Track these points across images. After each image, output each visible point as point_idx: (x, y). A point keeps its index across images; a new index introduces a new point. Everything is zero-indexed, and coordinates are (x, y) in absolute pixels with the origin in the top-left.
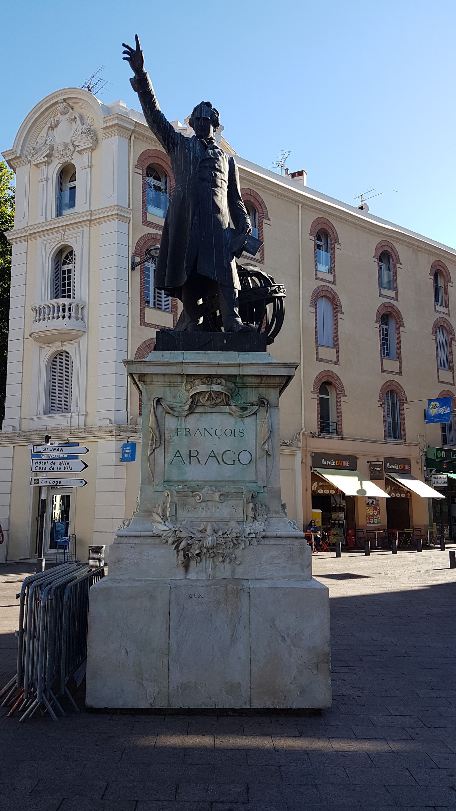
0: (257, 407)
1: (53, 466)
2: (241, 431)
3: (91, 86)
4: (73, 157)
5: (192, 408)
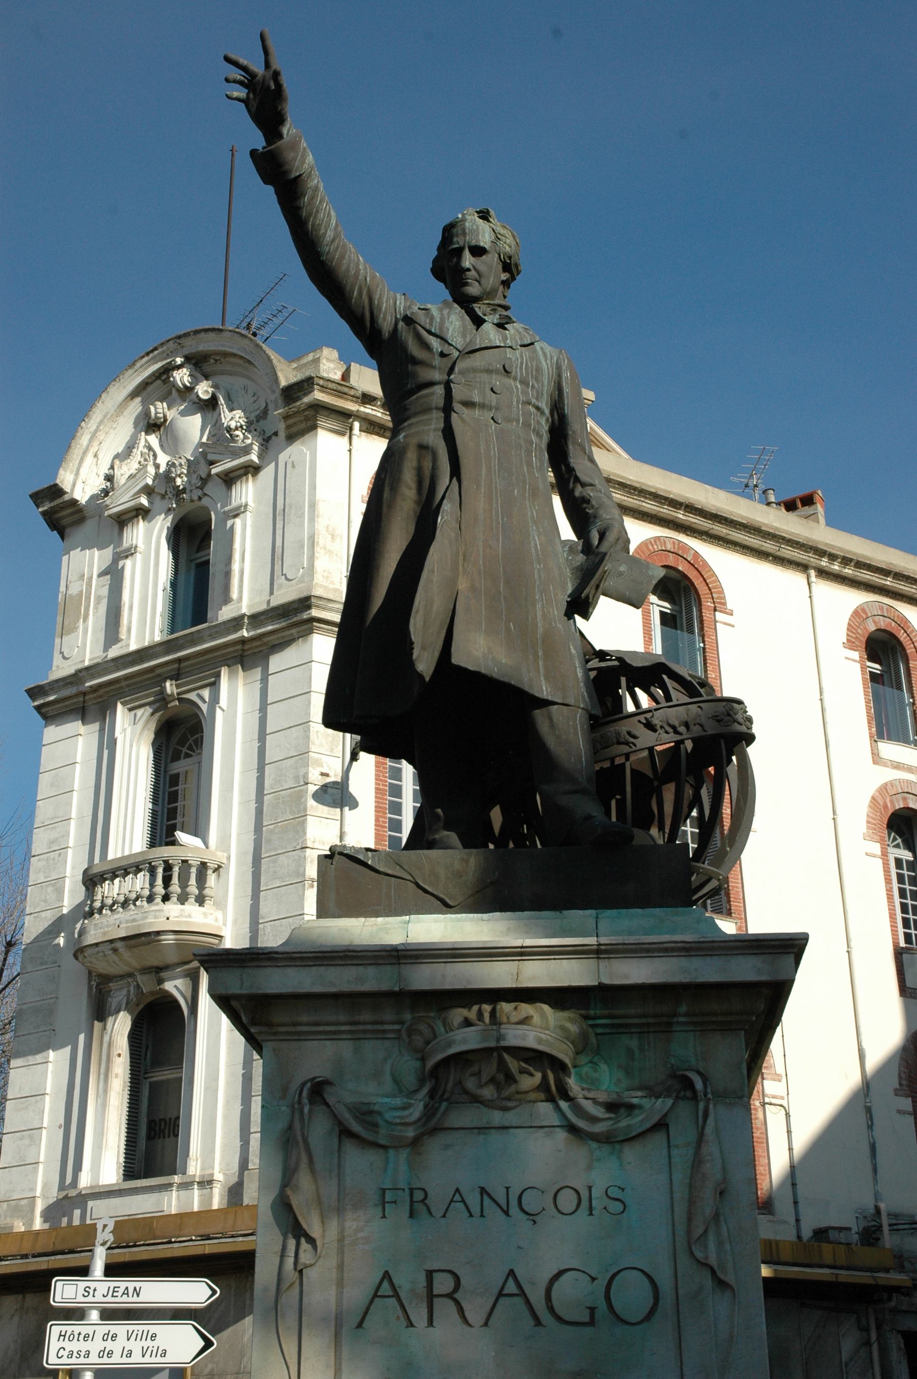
0: (670, 1102)
1: (109, 1345)
2: (613, 1192)
3: (254, 324)
4: (206, 491)
5: (434, 1114)
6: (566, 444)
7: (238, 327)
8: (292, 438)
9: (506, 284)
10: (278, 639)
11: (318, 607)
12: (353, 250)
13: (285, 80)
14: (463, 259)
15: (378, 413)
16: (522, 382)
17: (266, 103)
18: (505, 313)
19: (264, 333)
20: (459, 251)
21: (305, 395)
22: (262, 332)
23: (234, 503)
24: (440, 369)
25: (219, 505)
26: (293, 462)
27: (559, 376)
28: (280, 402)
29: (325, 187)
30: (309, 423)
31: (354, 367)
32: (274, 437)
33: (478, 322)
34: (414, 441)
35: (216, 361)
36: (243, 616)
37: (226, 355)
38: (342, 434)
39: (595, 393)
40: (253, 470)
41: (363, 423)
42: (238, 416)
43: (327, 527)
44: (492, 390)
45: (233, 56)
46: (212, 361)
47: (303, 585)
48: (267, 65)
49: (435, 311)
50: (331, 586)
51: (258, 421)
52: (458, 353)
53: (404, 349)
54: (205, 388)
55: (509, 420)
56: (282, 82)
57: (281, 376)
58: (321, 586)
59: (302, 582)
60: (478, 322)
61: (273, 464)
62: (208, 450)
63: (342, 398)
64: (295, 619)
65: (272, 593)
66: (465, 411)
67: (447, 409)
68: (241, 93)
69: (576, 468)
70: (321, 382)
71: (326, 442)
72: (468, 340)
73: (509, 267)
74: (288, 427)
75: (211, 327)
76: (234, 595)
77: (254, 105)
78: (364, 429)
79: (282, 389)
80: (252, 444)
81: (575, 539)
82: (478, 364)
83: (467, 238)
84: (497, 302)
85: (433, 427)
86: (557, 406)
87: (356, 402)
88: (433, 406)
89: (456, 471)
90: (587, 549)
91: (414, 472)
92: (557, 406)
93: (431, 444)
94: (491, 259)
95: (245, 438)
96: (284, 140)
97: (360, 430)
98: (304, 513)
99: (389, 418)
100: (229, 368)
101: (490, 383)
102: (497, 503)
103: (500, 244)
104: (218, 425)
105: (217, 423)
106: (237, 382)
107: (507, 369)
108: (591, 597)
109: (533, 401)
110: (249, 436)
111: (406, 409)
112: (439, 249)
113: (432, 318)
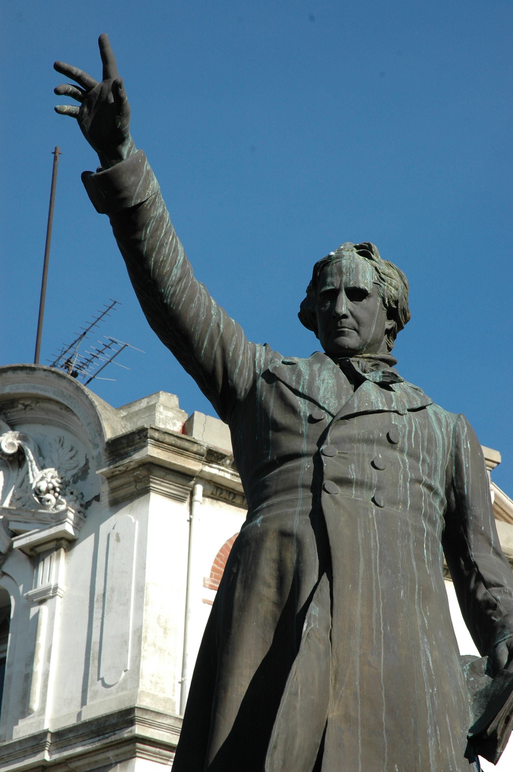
3: (75, 362)
6: (466, 532)
7: (54, 365)
8: (117, 504)
9: (391, 333)
10: (89, 764)
11: (143, 722)
12: (203, 291)
13: (128, 94)
14: (339, 303)
15: (227, 474)
16: (410, 455)
17: (103, 118)
18: (390, 370)
19: (87, 372)
20: (334, 294)
21: (136, 450)
22: (84, 372)
23: (41, 585)
24: (308, 437)
25: (21, 588)
26: (117, 535)
27: (457, 447)
28: (104, 458)
29: (171, 216)
30: (140, 486)
31: (199, 417)
32: (94, 503)
33: (357, 380)
34: (274, 526)
35: (26, 406)
36: (45, 733)
37: (38, 399)
38: (181, 499)
39: (501, 454)
40: (67, 543)
41: (208, 487)
42: (50, 475)
43: (159, 618)
44: (373, 464)
45: (65, 64)
46: (20, 406)
47: (125, 692)
48: (106, 75)
49: (302, 365)
50: (161, 695)
51: (75, 482)
52: (331, 418)
53: (263, 411)
54: (10, 440)
55: (394, 502)
56: (123, 95)
57: (105, 425)
58: (148, 695)
59: (123, 689)
60: (357, 380)
61: (92, 537)
62: (10, 517)
63: (182, 454)
64: (113, 738)
65: (84, 703)
66: (339, 491)
67: (317, 487)
68: (73, 106)
69: (479, 562)
70: (156, 435)
71: (160, 508)
72: (343, 402)
73: (395, 313)
74: (113, 490)
75: (20, 365)
76: (35, 705)
77: (88, 121)
78: (209, 493)
79: (108, 443)
80: (66, 510)
81: (477, 654)
82: (356, 432)
83: (344, 278)
84: (380, 355)
85: (298, 509)
86: (455, 485)
87: (200, 460)
88: (299, 483)
89: (326, 566)
90: (494, 669)
91: (274, 566)
92: (455, 485)
93: (295, 530)
94: (373, 305)
95: (59, 502)
96: (123, 162)
97: (204, 496)
98: (129, 600)
99: (239, 480)
100: (42, 415)
101: (370, 456)
102: (378, 607)
103: (385, 286)
104: (24, 487)
105: (24, 484)
106: (50, 434)
107: (392, 438)
108: (499, 732)
109: (425, 478)
110: (63, 500)
111: (265, 486)
112: (309, 290)
113: (299, 375)
